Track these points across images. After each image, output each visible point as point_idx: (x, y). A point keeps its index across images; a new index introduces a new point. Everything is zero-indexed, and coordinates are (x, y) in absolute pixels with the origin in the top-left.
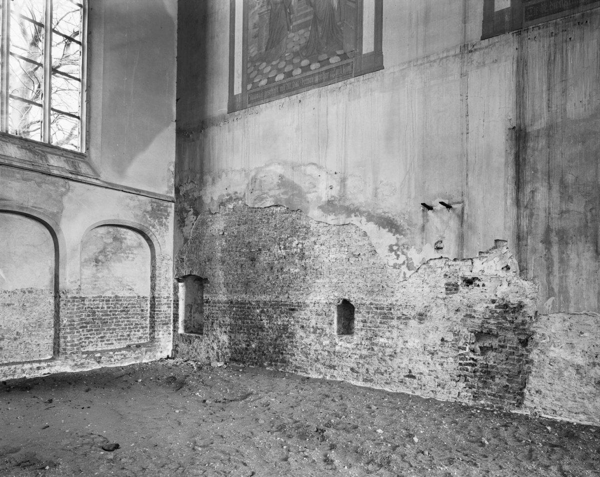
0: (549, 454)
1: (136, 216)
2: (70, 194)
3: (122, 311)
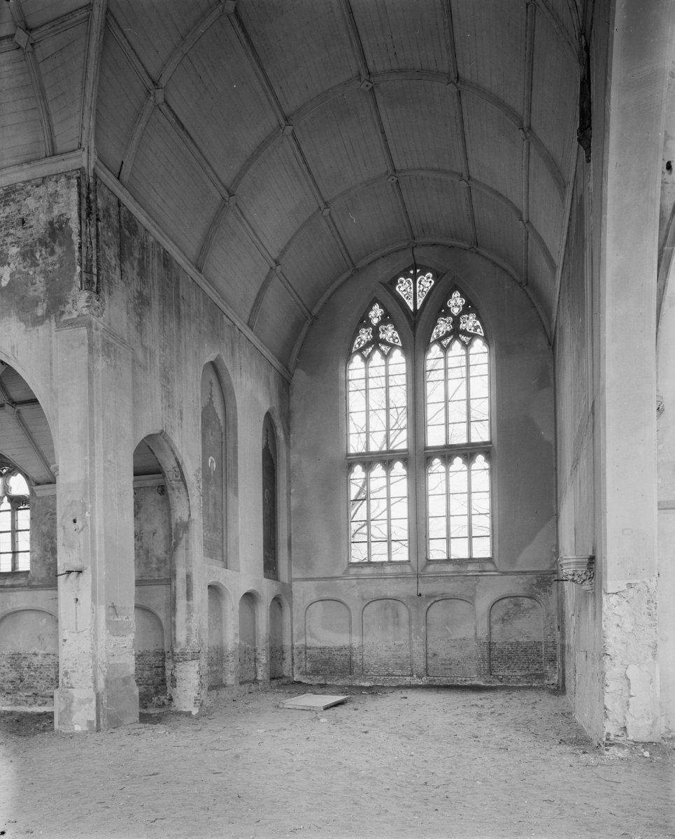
0: (41, 272)
1: (525, 589)
2: (479, 584)
3: (522, 651)
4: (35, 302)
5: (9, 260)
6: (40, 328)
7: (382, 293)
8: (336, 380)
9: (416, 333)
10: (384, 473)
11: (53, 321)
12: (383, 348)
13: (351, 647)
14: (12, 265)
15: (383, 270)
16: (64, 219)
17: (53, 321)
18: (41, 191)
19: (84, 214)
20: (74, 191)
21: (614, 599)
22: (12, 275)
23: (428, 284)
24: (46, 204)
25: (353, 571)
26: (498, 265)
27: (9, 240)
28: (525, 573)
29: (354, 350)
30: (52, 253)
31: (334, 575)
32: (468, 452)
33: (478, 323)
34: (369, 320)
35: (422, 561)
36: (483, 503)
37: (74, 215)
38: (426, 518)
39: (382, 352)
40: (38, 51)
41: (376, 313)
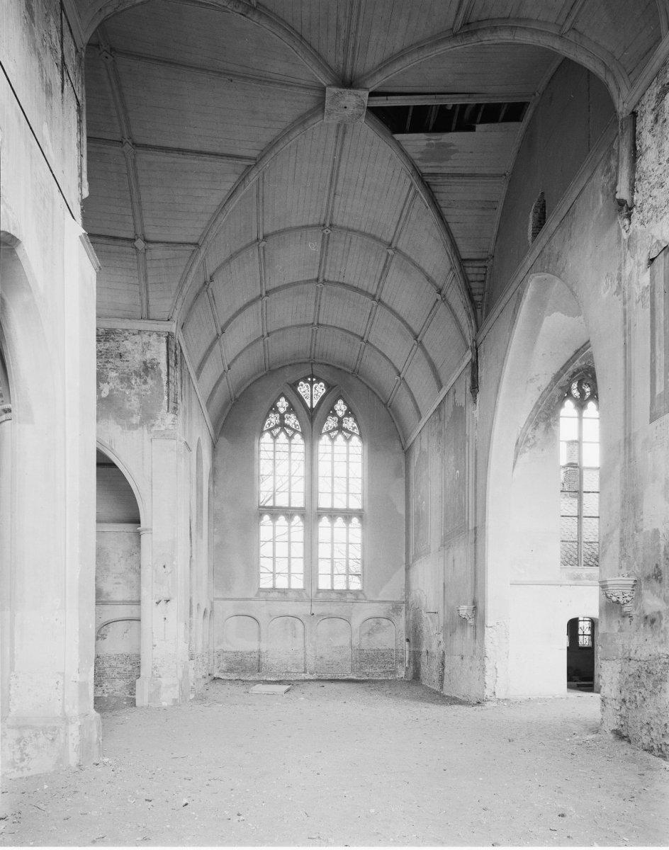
0: (135, 394)
4: (131, 414)
5: (109, 380)
6: (135, 432)
7: (290, 393)
8: (252, 450)
9: (312, 421)
10: (286, 523)
11: (145, 428)
12: (288, 431)
13: (259, 651)
14: (111, 384)
15: (290, 376)
16: (155, 362)
17: (145, 428)
18: (137, 338)
19: (172, 363)
20: (164, 346)
21: (489, 629)
22: (111, 391)
23: (321, 391)
24: (140, 348)
25: (262, 594)
26: (371, 389)
27: (109, 366)
28: (385, 602)
29: (265, 429)
30: (145, 382)
31: (248, 597)
32: (347, 515)
33: (355, 425)
34: (277, 408)
35: (314, 590)
36: (356, 552)
37: (163, 360)
38: (305, 558)
39: (287, 434)
40: (148, 253)
41: (282, 404)
